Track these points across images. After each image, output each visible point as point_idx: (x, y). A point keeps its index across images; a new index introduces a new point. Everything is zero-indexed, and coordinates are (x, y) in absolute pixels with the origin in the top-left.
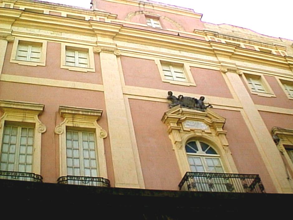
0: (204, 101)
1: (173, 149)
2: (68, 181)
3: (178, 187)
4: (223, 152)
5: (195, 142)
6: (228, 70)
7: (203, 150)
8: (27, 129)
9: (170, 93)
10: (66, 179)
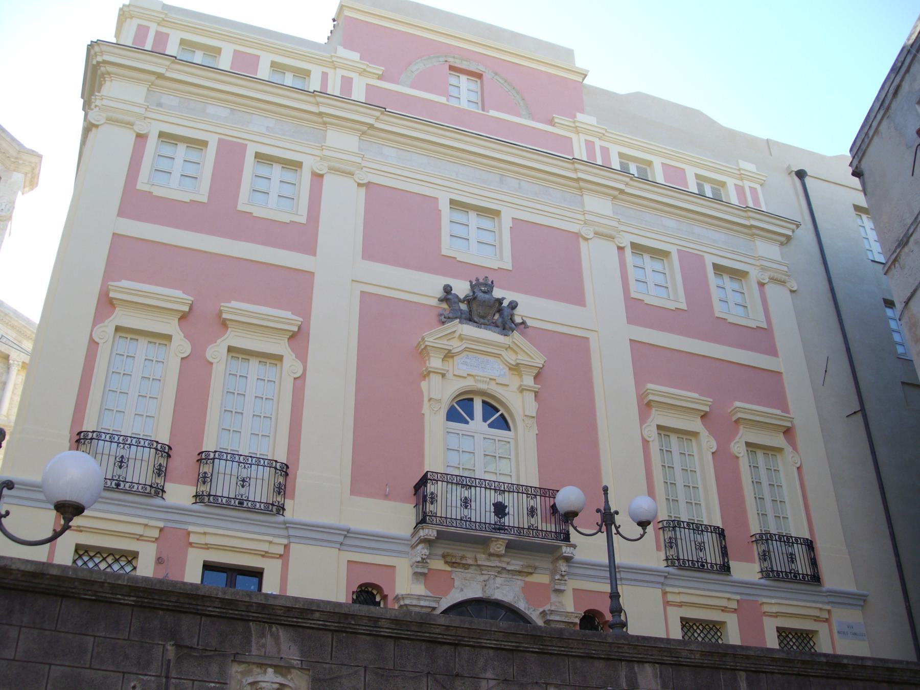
0: (517, 311)
1: (423, 412)
2: (216, 460)
3: (413, 487)
4: (520, 425)
5: (471, 400)
6: (596, 233)
7: (485, 420)
8: (155, 343)
9: (448, 289)
10: (212, 455)
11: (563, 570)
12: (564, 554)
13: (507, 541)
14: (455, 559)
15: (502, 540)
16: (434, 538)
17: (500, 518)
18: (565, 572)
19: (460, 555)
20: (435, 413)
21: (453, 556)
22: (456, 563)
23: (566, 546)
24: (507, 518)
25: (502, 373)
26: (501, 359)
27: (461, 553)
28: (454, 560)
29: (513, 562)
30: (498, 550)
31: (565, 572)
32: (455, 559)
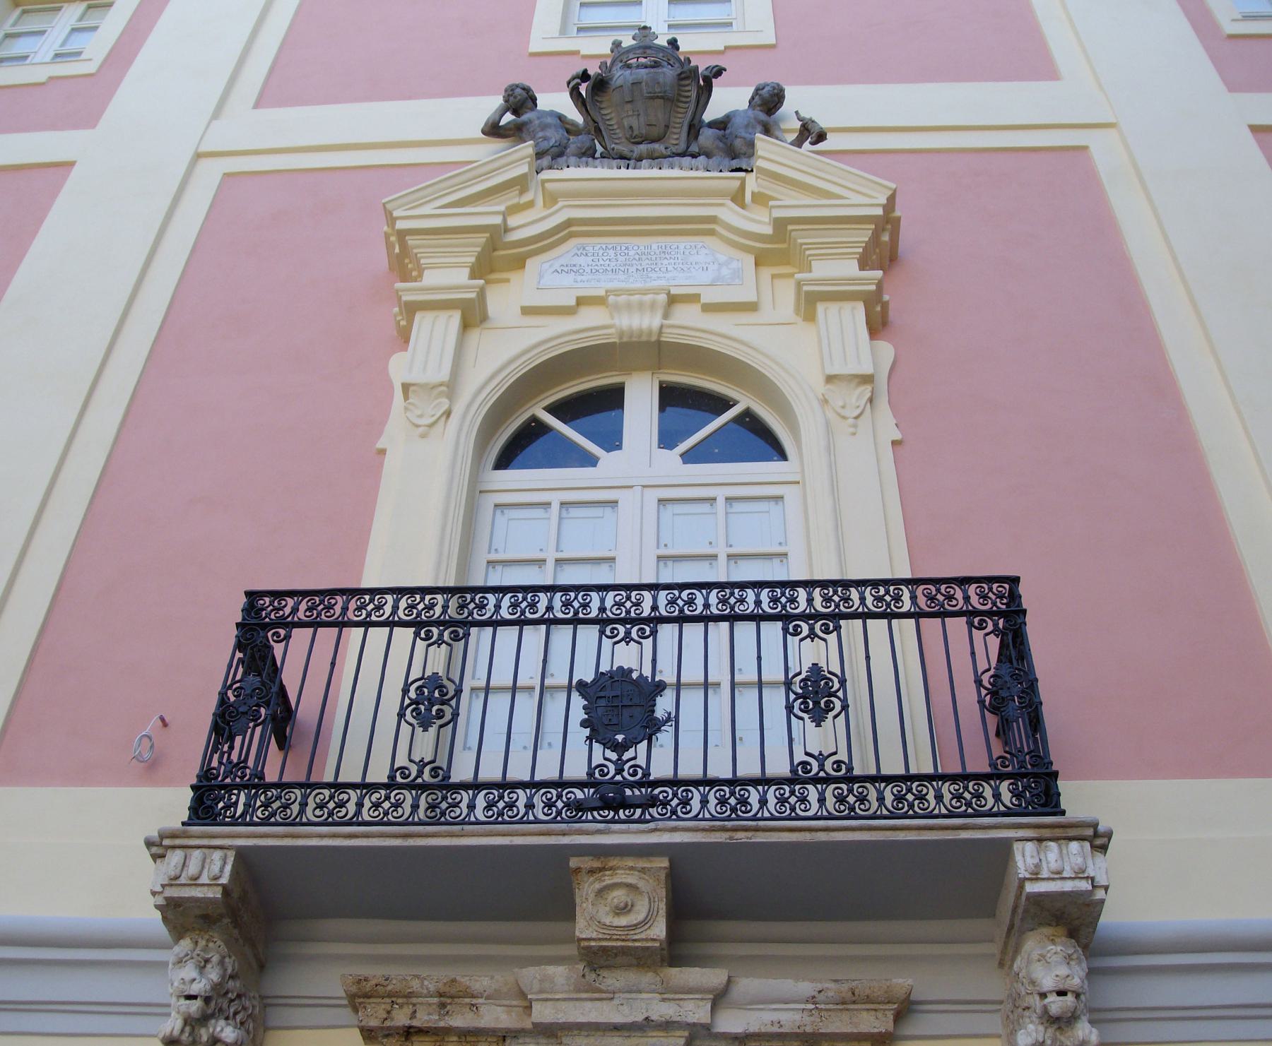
7: (667, 440)
11: (1048, 983)
12: (1030, 888)
13: (664, 863)
14: (408, 1010)
15: (630, 862)
16: (216, 893)
17: (620, 748)
18: (1061, 993)
19: (432, 988)
20: (423, 436)
21: (390, 995)
22: (421, 1031)
23: (1040, 840)
24: (665, 738)
25: (725, 272)
26: (722, 238)
27: (434, 978)
28: (401, 1018)
29: (748, 985)
30: (623, 921)
31: (1061, 993)
32: (408, 1010)
